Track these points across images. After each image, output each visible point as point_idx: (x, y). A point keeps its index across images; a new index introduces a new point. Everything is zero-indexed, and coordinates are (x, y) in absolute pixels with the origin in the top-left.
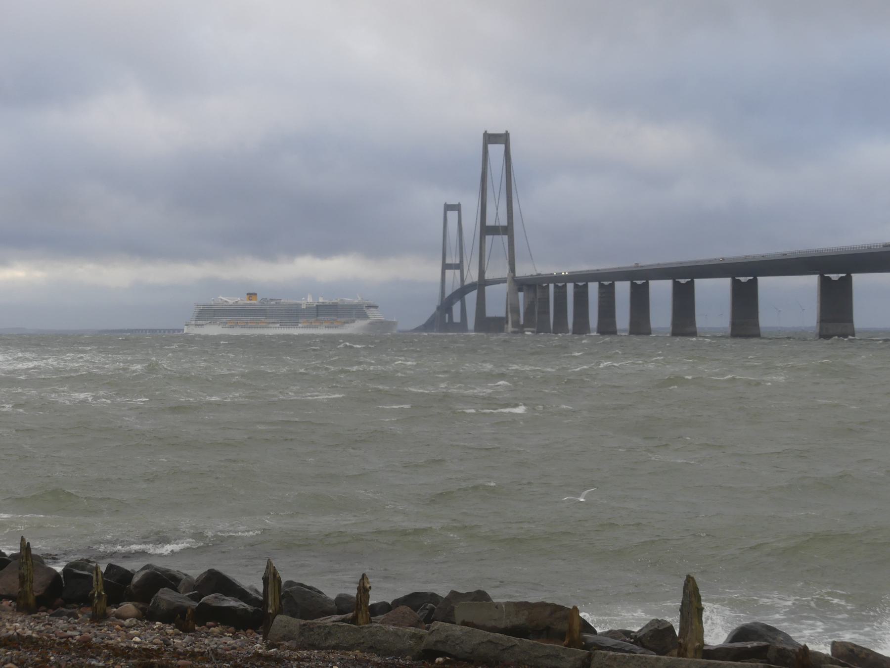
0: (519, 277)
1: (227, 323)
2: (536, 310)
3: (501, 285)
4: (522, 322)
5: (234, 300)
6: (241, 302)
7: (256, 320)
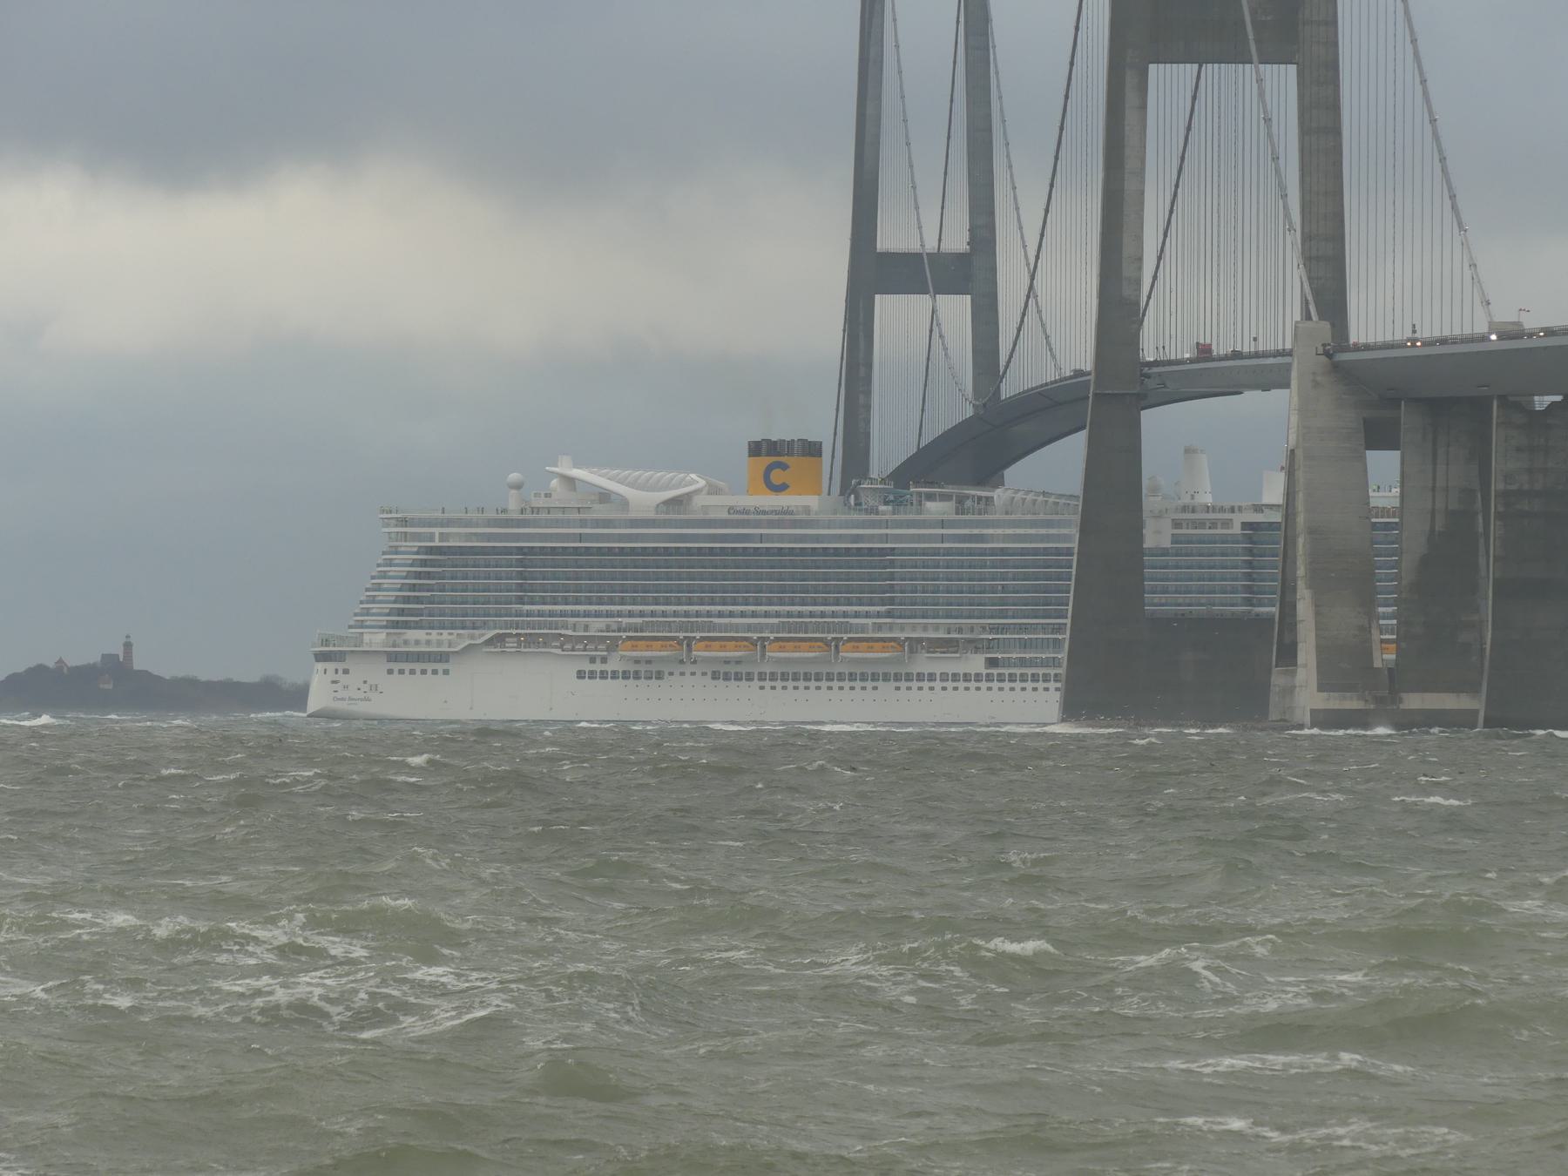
0: (1367, 347)
1: (613, 645)
2: (1489, 571)
3: (1252, 401)
4: (1385, 657)
5: (667, 487)
6: (715, 505)
7: (818, 627)
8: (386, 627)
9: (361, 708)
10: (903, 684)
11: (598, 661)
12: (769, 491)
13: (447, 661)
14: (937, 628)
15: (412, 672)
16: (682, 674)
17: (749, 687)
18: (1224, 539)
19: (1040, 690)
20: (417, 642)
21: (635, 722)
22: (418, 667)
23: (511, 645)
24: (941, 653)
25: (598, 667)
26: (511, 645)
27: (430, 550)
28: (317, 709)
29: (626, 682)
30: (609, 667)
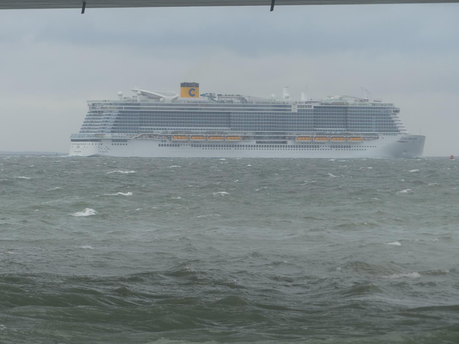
8: (111, 132)
9: (106, 154)
10: (237, 148)
11: (164, 141)
12: (191, 96)
13: (127, 141)
14: (242, 133)
15: (118, 144)
16: (184, 145)
17: (195, 148)
18: (309, 110)
19: (229, 149)
20: (116, 136)
21: (26, 155)
22: (120, 143)
23: (144, 137)
24: (247, 140)
25: (164, 143)
26: (144, 137)
28: (94, 154)
29: (171, 147)
30: (166, 143)
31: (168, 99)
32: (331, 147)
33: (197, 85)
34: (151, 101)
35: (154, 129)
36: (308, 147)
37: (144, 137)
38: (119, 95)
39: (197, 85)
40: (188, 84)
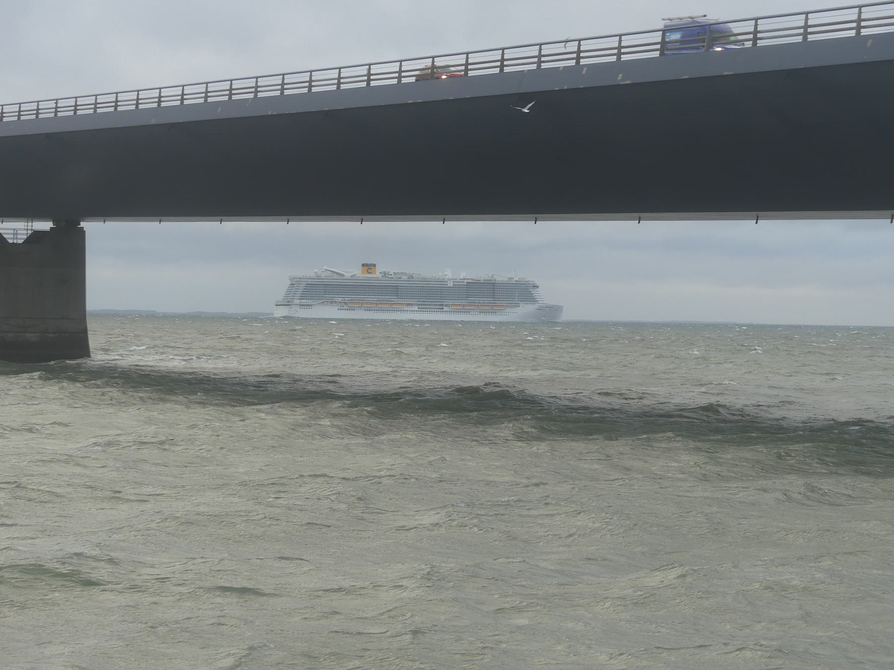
25: (342, 308)
27: (307, 284)
31: (348, 275)
32: (480, 312)
33: (375, 265)
34: (336, 276)
35: (335, 297)
36: (463, 312)
37: (325, 303)
38: (315, 272)
39: (375, 265)
40: (367, 264)
